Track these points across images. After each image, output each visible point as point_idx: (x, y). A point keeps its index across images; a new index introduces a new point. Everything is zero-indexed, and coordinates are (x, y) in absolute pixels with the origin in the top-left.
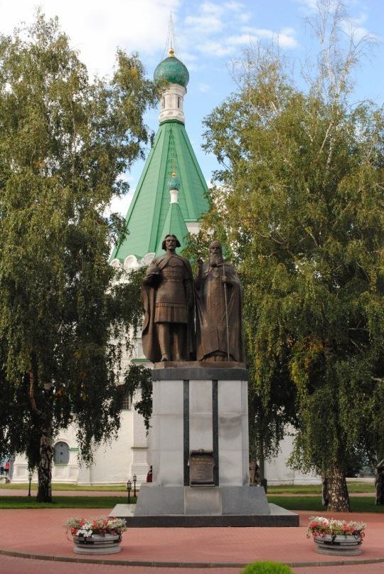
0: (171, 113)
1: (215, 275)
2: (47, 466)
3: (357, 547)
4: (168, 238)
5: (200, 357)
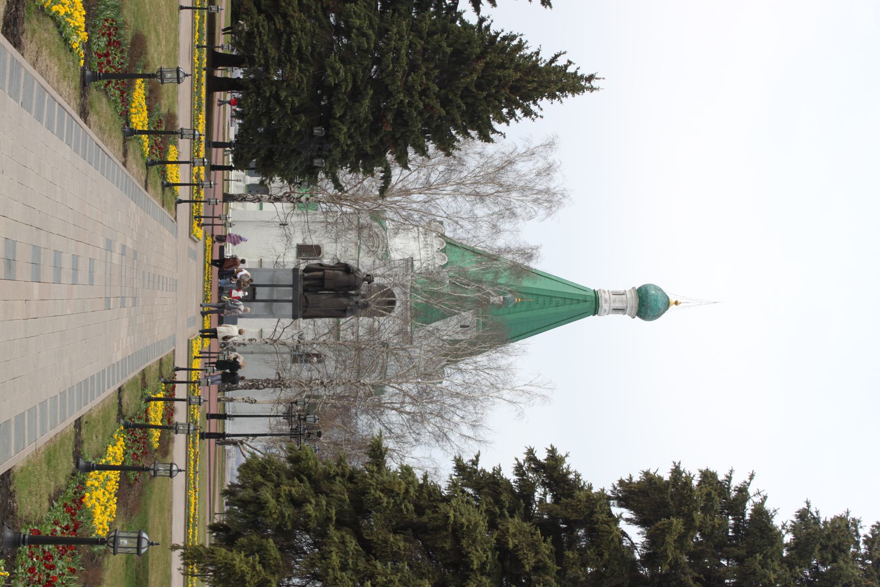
0: (606, 301)
1: (351, 303)
5: (305, 294)
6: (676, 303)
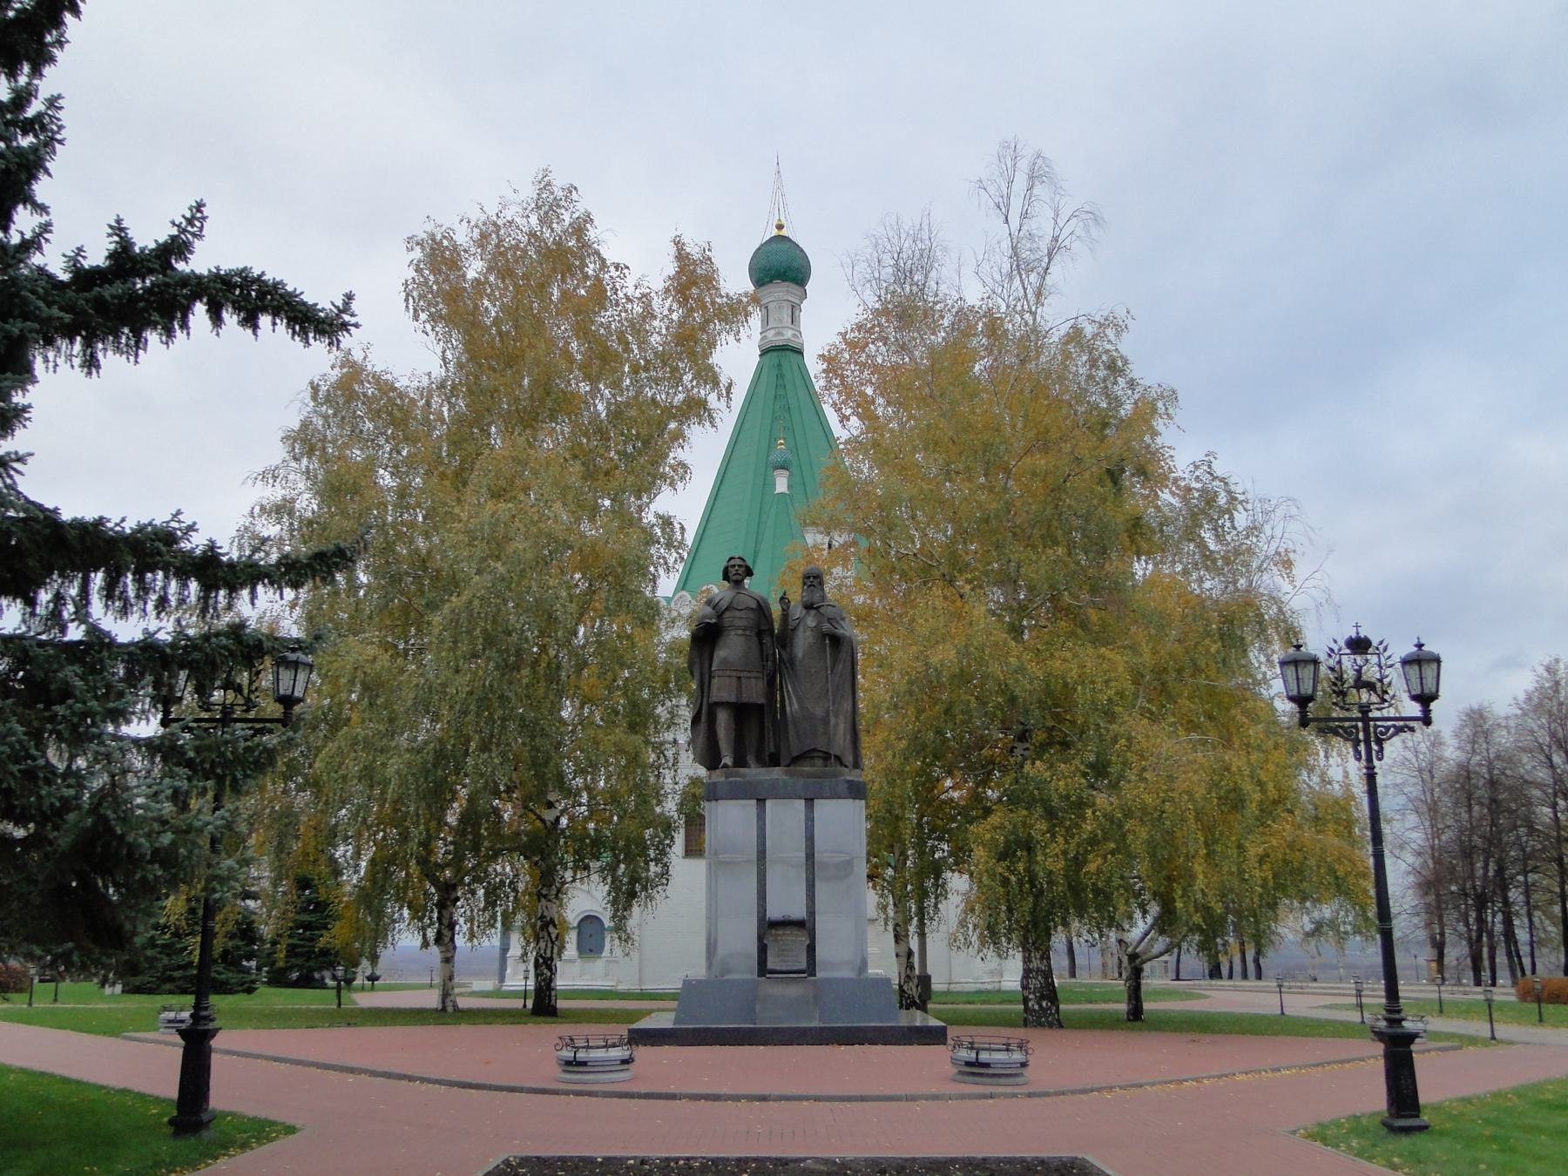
2: (549, 952)
3: (1019, 1071)
4: (732, 562)
5: (784, 760)
6: (780, 227)
